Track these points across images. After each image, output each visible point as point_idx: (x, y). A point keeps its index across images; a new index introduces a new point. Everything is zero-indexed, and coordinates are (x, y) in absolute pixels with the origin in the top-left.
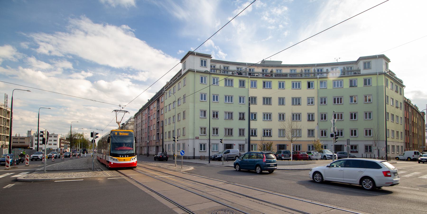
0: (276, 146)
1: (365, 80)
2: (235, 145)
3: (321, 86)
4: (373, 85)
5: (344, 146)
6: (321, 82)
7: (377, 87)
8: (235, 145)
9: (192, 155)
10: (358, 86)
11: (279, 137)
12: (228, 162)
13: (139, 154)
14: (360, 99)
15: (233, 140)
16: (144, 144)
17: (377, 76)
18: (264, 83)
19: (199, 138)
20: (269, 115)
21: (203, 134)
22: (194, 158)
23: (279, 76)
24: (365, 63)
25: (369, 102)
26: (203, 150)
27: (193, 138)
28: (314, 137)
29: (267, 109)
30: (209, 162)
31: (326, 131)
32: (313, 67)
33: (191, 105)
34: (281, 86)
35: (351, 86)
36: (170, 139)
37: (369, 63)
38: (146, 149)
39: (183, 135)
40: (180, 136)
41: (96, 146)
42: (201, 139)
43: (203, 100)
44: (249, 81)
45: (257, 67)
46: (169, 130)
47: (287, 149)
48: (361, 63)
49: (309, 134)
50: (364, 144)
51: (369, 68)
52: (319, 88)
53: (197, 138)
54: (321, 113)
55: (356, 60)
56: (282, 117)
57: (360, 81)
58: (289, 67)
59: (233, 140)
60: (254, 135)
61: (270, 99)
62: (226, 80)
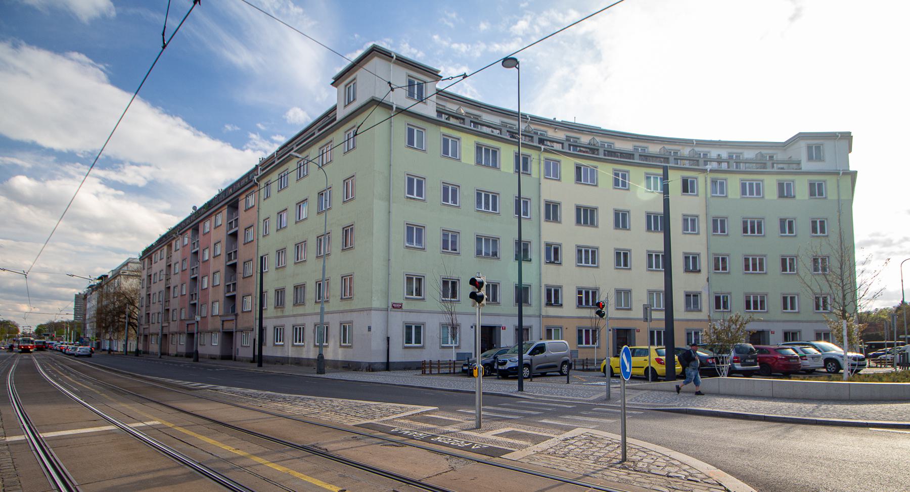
0: (611, 332)
1: (812, 185)
2: (504, 328)
3: (714, 191)
4: (829, 198)
5: (770, 332)
6: (714, 182)
7: (839, 202)
8: (504, 328)
9: (382, 359)
10: (798, 197)
11: (617, 309)
12: (531, 381)
13: (159, 354)
14: (803, 227)
15: (498, 315)
16: (174, 327)
17: (839, 178)
18: (578, 168)
19: (403, 308)
20: (585, 251)
21: (414, 296)
22: (388, 366)
23: (612, 155)
24: (809, 148)
25: (822, 234)
26: (413, 344)
27: (384, 306)
28: (700, 311)
29: (586, 236)
30: (521, 388)
31: (727, 297)
32: (686, 146)
33: (379, 207)
34: (620, 182)
35: (781, 195)
36: (283, 311)
37: (818, 148)
38: (183, 339)
39: (342, 298)
40: (327, 301)
41: (17, 333)
42: (410, 311)
43: (415, 196)
44: (540, 159)
45: (553, 128)
46: (280, 285)
47: (771, 342)
48: (803, 144)
49: (688, 303)
50: (814, 330)
51: (819, 158)
52: (709, 196)
53: (397, 307)
54: (715, 254)
55: (783, 139)
56: (622, 258)
57: (801, 187)
58: (630, 141)
59: (498, 315)
60: (553, 302)
61: (593, 211)
62: (479, 148)
